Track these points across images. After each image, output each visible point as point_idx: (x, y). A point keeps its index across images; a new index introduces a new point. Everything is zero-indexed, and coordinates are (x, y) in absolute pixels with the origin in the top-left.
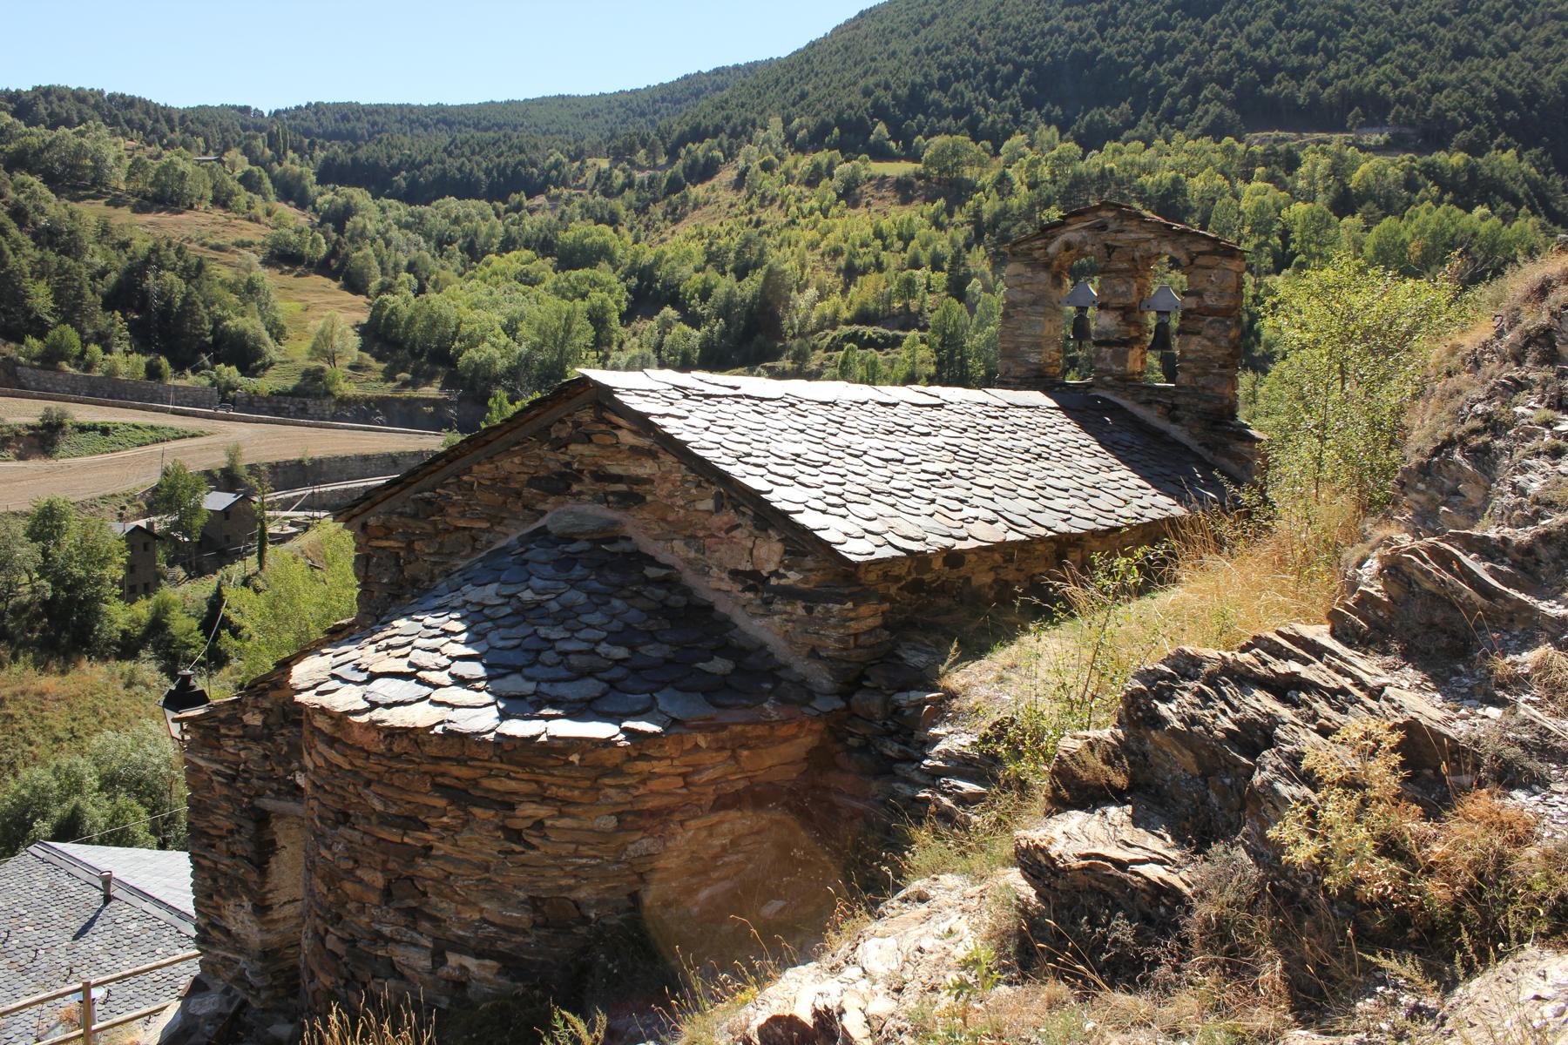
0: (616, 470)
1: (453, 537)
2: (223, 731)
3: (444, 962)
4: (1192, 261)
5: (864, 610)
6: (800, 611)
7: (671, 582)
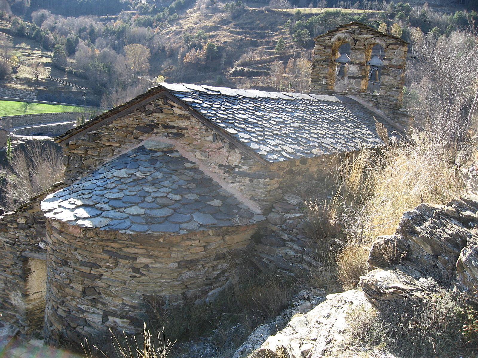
0: (172, 124)
1: (104, 149)
2: (9, 225)
3: (107, 320)
4: (387, 46)
5: (273, 181)
6: (247, 180)
7: (195, 170)
